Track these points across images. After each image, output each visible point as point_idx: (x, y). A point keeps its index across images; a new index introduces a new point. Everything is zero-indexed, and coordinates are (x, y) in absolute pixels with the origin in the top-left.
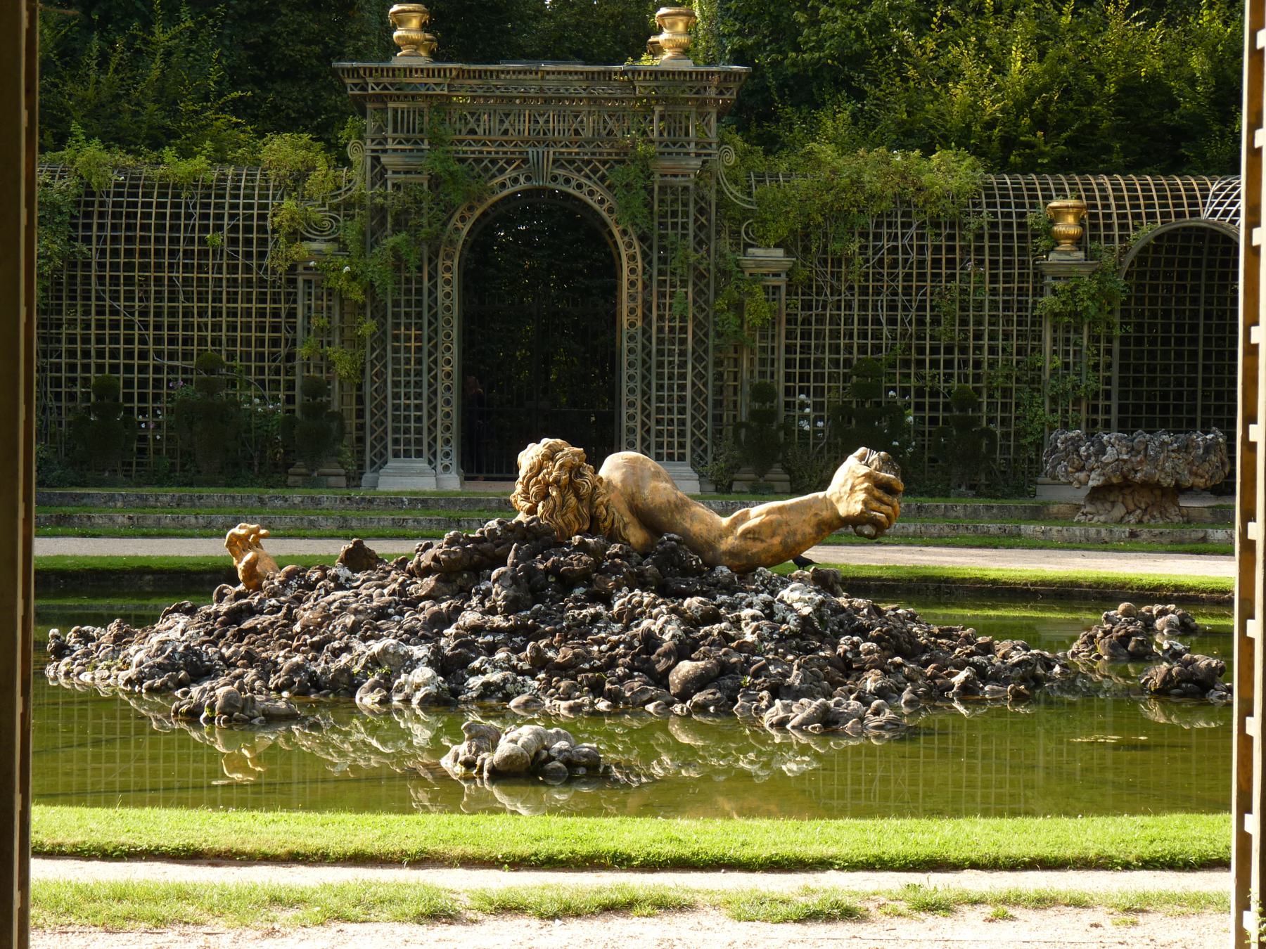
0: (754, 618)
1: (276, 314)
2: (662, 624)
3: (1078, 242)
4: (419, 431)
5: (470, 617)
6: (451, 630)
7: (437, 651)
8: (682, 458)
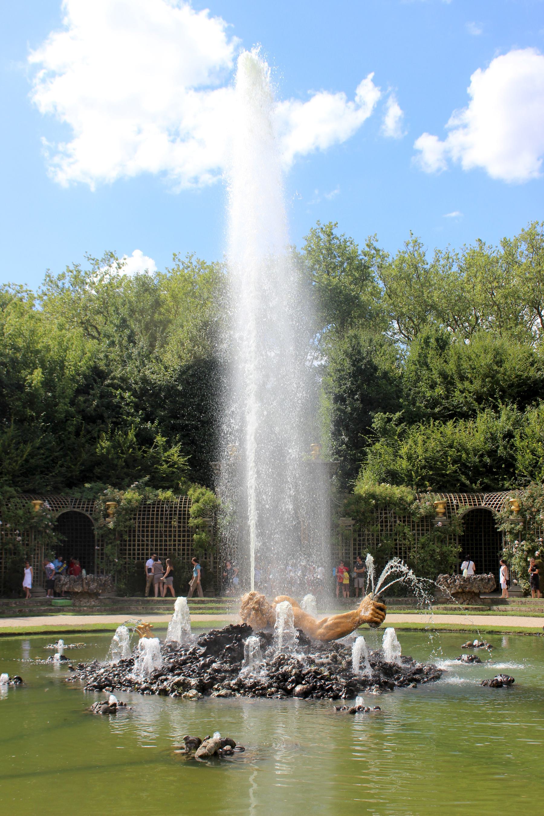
3: (444, 514)
7: (201, 681)
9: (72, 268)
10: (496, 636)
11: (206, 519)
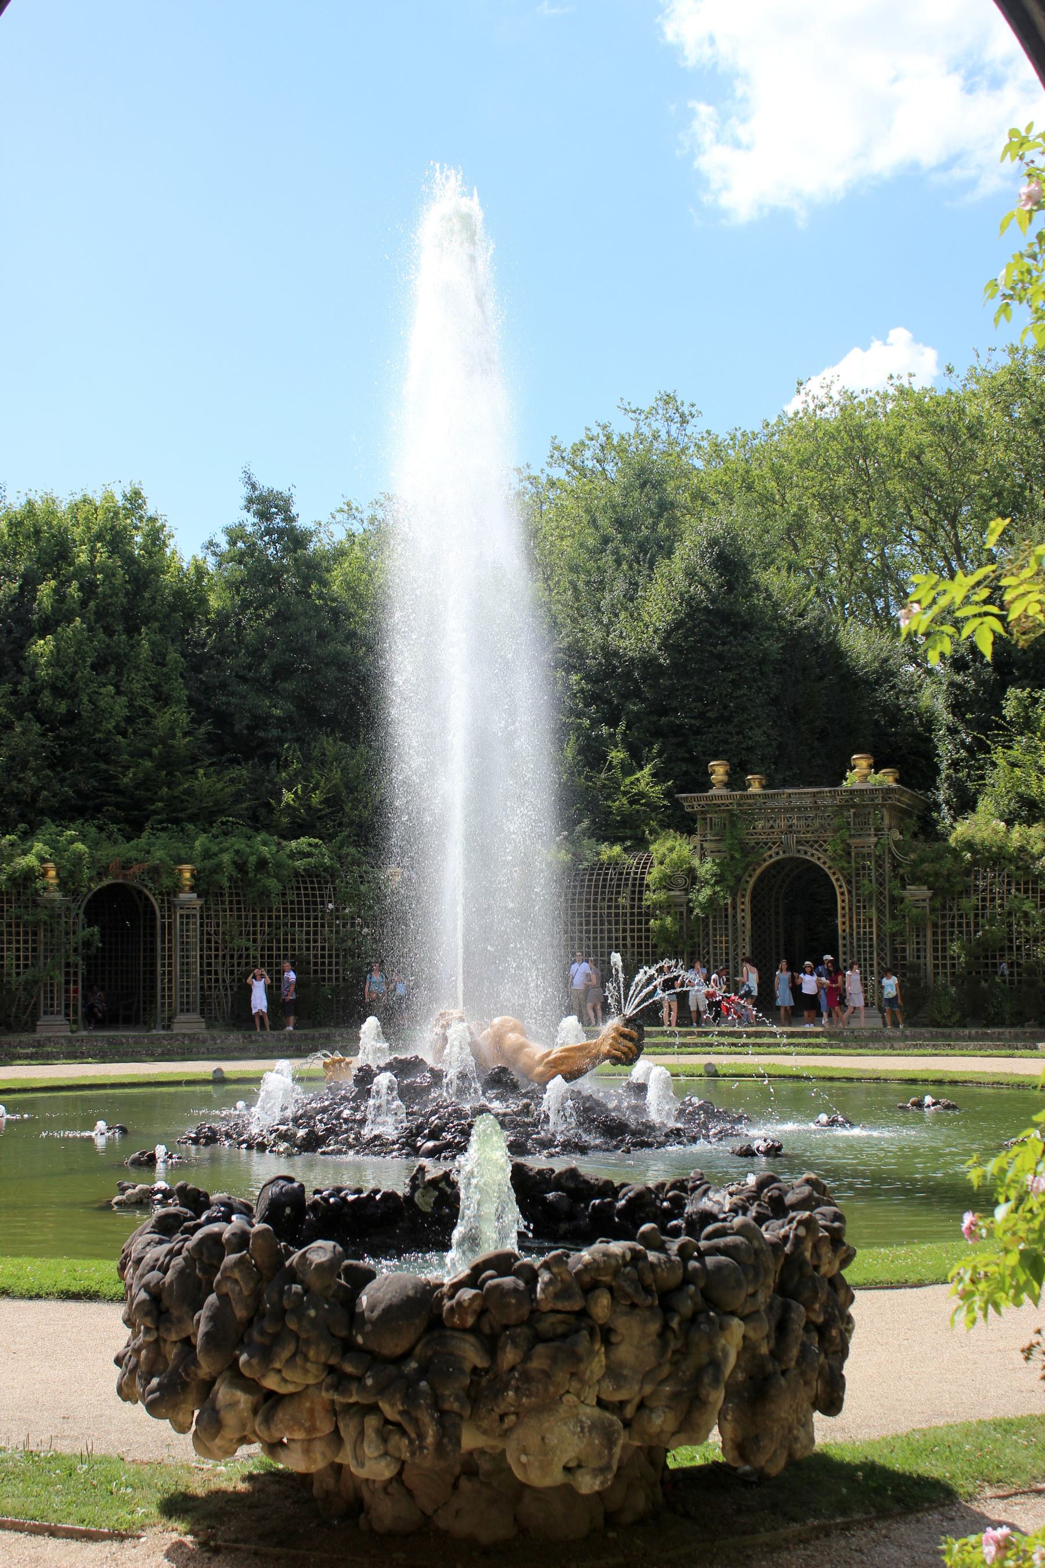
9: (596, 431)
10: (882, 1085)
11: (672, 893)
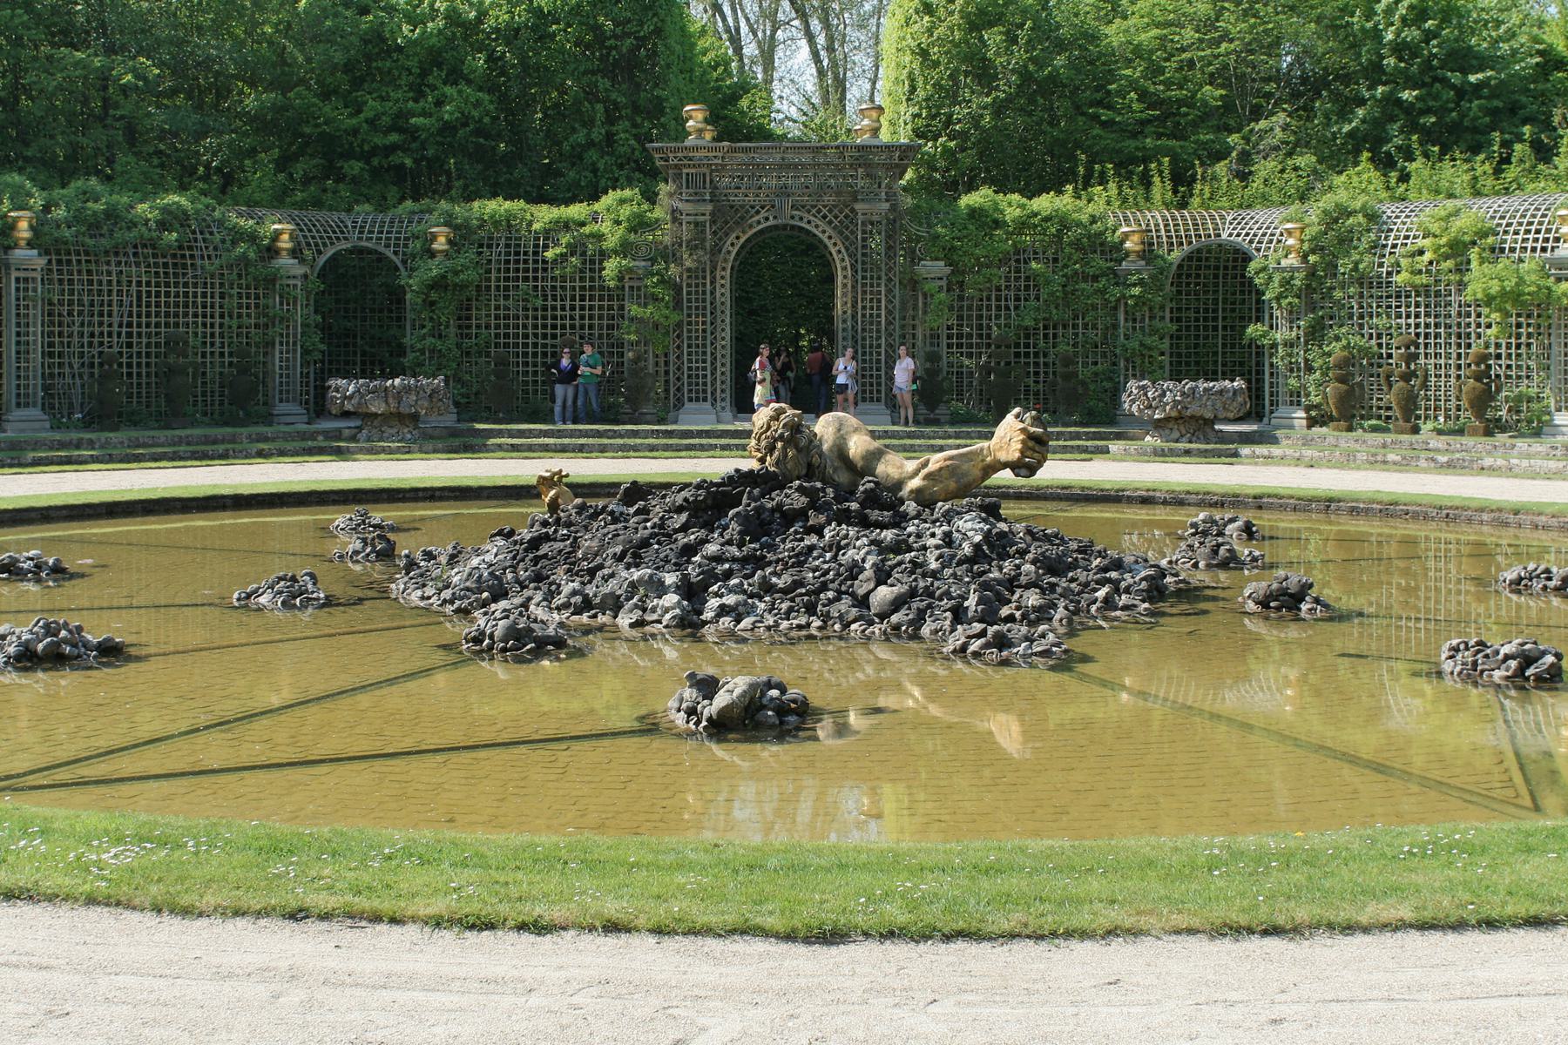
0: (937, 547)
1: (610, 308)
2: (860, 550)
4: (705, 384)
5: (712, 548)
6: (697, 559)
7: (685, 577)
8: (879, 400)
